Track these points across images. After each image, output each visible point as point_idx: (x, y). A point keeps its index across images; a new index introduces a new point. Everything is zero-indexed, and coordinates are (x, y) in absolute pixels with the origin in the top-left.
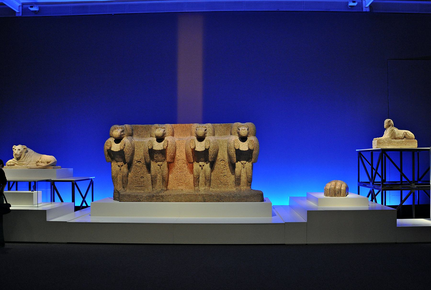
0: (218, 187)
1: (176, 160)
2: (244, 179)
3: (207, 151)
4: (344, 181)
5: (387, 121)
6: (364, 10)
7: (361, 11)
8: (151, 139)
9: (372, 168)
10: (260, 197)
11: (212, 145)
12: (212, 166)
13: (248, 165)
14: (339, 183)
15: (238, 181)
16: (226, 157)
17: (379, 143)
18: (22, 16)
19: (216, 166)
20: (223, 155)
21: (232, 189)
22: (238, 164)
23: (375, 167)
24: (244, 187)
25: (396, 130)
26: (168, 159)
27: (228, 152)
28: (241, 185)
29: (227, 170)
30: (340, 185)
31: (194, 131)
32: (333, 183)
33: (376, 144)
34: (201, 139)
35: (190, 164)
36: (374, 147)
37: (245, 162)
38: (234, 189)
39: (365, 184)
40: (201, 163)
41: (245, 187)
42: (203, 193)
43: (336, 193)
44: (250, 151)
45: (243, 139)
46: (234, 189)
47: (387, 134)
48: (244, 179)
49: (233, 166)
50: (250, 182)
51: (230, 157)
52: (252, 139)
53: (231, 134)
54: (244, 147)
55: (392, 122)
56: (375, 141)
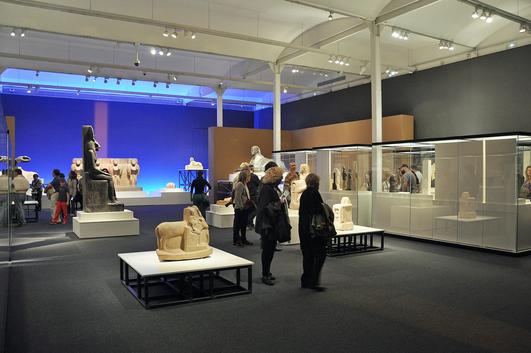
0: (123, 186)
2: (133, 182)
3: (119, 170)
4: (174, 183)
5: (191, 158)
6: (184, 105)
7: (182, 105)
9: (185, 178)
10: (141, 189)
12: (120, 176)
13: (135, 176)
14: (172, 183)
15: (131, 183)
16: (126, 173)
17: (188, 167)
18: (3, 93)
20: (125, 172)
21: (129, 186)
22: (131, 176)
23: (186, 177)
24: (133, 185)
25: (195, 162)
27: (127, 171)
28: (132, 184)
29: (127, 178)
30: (173, 184)
32: (170, 183)
33: (187, 168)
34: (116, 165)
35: (129, 177)
36: (186, 169)
37: (134, 175)
38: (130, 186)
39: (182, 185)
40: (115, 175)
41: (134, 185)
42: (117, 188)
43: (171, 187)
44: (137, 171)
45: (134, 165)
46: (130, 186)
47: (191, 163)
48: (133, 182)
49: (129, 177)
50: (136, 183)
51: (128, 173)
52: (137, 165)
53: (128, 163)
54: (134, 169)
55: (193, 159)
56: (186, 166)
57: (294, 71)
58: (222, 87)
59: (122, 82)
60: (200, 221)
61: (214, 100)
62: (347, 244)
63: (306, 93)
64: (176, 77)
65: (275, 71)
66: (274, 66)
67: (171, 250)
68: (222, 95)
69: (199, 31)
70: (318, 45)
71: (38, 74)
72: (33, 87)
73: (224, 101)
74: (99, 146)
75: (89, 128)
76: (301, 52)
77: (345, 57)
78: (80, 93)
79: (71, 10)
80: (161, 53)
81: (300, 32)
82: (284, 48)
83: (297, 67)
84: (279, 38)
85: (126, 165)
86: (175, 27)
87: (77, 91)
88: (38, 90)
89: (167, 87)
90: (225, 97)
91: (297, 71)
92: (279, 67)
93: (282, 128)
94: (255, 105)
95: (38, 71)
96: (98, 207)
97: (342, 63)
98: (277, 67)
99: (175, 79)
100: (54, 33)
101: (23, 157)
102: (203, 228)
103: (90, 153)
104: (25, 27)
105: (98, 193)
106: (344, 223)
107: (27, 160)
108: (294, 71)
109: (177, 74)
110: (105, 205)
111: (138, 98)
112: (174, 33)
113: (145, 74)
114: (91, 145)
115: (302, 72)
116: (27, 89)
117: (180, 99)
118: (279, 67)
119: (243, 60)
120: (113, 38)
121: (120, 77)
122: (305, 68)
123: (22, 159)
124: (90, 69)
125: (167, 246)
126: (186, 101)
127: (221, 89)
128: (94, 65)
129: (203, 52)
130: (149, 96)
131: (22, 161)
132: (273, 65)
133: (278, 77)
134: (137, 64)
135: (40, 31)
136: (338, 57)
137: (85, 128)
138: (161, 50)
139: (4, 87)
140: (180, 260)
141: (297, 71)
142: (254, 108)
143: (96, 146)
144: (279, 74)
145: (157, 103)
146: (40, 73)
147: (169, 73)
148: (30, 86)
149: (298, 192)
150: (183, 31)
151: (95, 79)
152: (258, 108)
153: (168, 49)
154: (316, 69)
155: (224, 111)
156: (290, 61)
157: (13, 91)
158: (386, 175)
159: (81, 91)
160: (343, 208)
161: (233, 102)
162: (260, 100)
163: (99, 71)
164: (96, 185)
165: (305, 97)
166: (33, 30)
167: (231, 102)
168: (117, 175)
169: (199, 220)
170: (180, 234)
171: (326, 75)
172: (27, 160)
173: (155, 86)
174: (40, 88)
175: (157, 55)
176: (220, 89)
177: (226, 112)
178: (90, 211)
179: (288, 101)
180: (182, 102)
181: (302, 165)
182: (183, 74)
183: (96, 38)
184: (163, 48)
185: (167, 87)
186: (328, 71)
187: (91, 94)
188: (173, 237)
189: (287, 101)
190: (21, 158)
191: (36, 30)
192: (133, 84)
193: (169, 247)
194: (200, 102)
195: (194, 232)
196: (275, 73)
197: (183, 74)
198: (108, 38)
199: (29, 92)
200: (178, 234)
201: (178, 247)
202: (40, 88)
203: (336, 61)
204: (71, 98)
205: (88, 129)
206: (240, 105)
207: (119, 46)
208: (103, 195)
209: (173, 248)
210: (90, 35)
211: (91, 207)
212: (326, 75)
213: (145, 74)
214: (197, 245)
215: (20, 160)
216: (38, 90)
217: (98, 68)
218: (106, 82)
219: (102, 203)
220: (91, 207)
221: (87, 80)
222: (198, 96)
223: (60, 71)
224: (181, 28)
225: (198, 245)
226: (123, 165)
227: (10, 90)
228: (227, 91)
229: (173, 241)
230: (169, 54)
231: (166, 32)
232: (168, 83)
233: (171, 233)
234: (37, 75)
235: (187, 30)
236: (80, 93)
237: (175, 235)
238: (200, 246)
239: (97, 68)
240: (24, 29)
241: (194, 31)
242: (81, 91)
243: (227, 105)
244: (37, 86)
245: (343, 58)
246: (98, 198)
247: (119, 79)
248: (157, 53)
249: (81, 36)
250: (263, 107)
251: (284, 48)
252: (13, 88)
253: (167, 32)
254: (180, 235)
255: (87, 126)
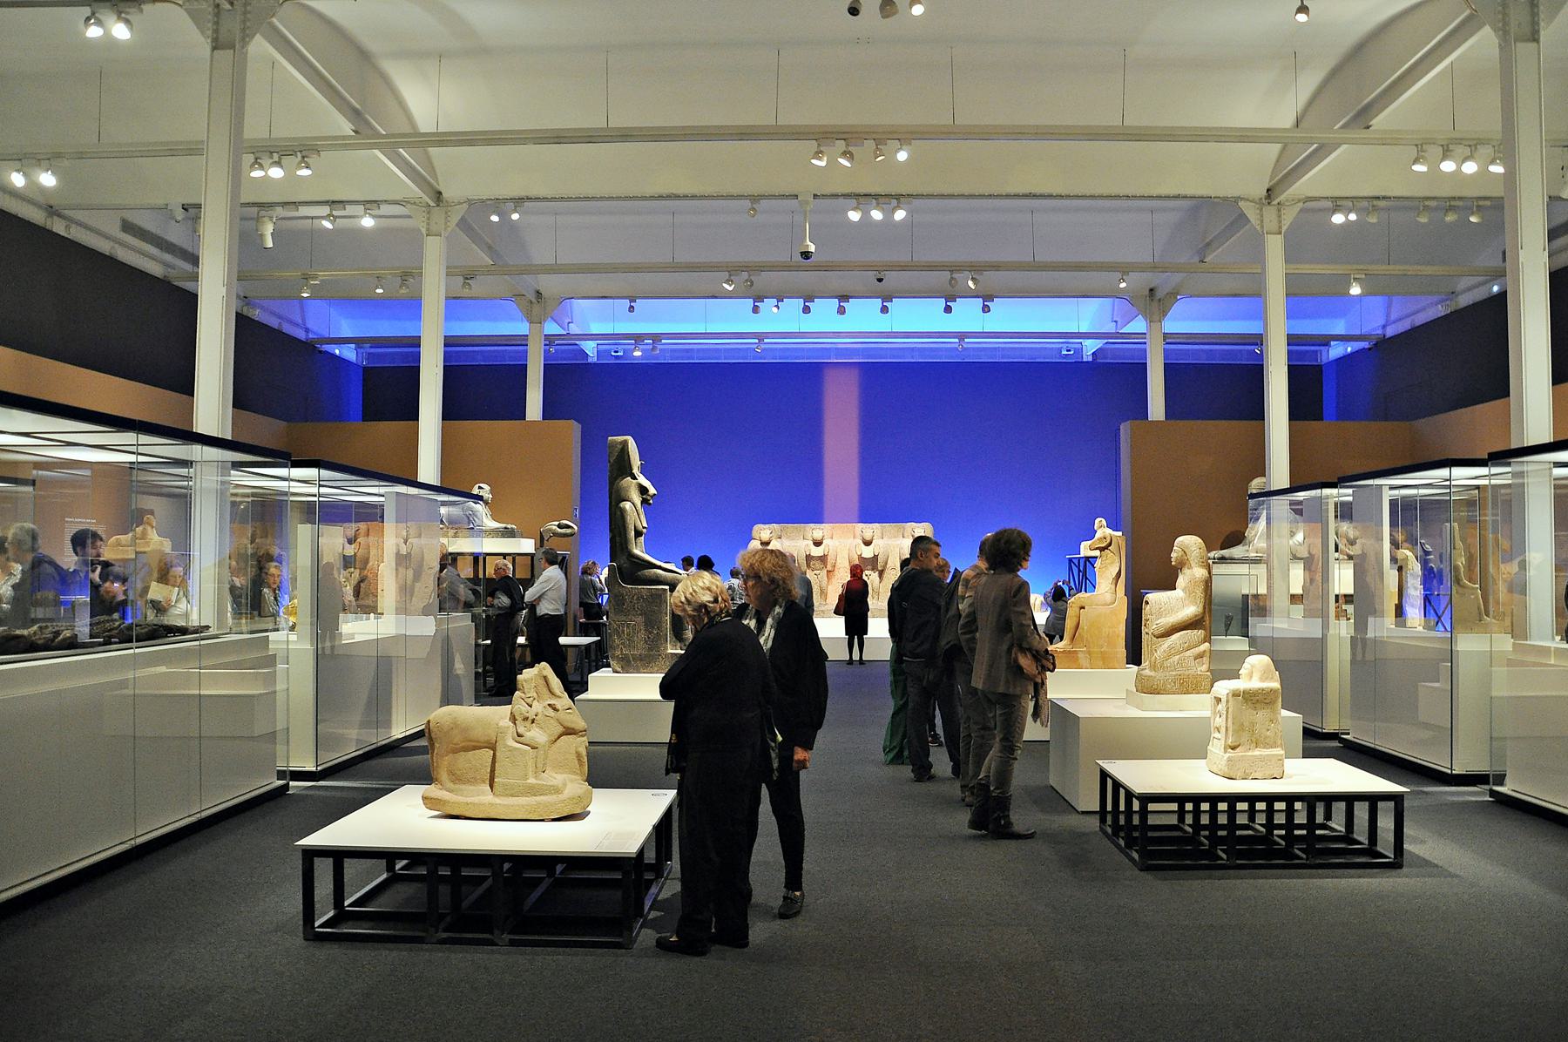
1: (836, 569)
3: (876, 557)
8: (806, 542)
11: (882, 551)
19: (885, 575)
26: (829, 568)
31: (858, 532)
34: (868, 543)
55: (1104, 522)
57: (1338, 219)
58: (1159, 294)
59: (851, 305)
60: (550, 709)
61: (522, 341)
62: (1205, 830)
63: (1469, 289)
64: (973, 279)
65: (1262, 227)
66: (1261, 210)
67: (463, 787)
68: (1161, 322)
69: (919, 136)
70: (1363, 117)
71: (633, 307)
72: (646, 341)
73: (550, 340)
74: (652, 491)
75: (621, 443)
76: (1322, 151)
77: (1432, 142)
78: (763, 346)
79: (559, 138)
80: (877, 215)
81: (1309, 82)
82: (1279, 146)
83: (1351, 204)
84: (1245, 115)
85: (899, 542)
86: (874, 136)
87: (757, 341)
88: (659, 347)
89: (984, 311)
90: (1176, 323)
91: (1353, 217)
92: (1279, 210)
93: (1294, 415)
94: (1327, 344)
95: (633, 300)
96: (641, 658)
97: (1470, 168)
98: (1270, 213)
99: (971, 284)
100: (587, 199)
101: (557, 523)
102: (560, 729)
103: (623, 512)
104: (1042, 192)
105: (640, 619)
106: (1239, 752)
107: (569, 531)
108: (1338, 219)
109: (976, 269)
110: (660, 655)
111: (947, 349)
112: (844, 154)
113: (880, 280)
114: (627, 489)
115: (1373, 219)
116: (633, 347)
117: (1073, 343)
118: (1279, 210)
119: (1194, 202)
120: (735, 192)
121: (989, 293)
122: (1382, 204)
123: (554, 527)
124: (727, 282)
125: (451, 773)
126: (1090, 347)
127: (1160, 300)
128: (737, 268)
129: (1008, 196)
130: (957, 340)
131: (556, 534)
132: (1257, 206)
133: (1275, 247)
134: (806, 255)
135: (553, 199)
136: (1451, 147)
137: (614, 444)
138: (877, 207)
139: (600, 347)
140: (480, 817)
141: (1353, 217)
142: (1324, 353)
143: (643, 490)
144: (1280, 233)
145: (1002, 358)
146: (638, 304)
147: (954, 268)
148: (638, 338)
149: (1156, 633)
150: (870, 144)
151: (777, 307)
152: (1336, 351)
153: (899, 199)
154: (1427, 203)
155: (1168, 368)
156: (1305, 185)
157: (618, 354)
158: (683, 560)
159: (766, 341)
160: (1233, 695)
161: (1247, 341)
162: (1339, 328)
163: (752, 283)
164: (635, 597)
165: (1464, 300)
166: (537, 199)
167: (1243, 341)
168: (873, 570)
169: (549, 705)
170: (485, 742)
171: (1473, 219)
172: (569, 531)
173: (948, 309)
174: (663, 341)
175: (1348, 224)
176: (1155, 301)
177: (453, 376)
178: (619, 670)
179: (1416, 320)
180: (1079, 351)
181: (1180, 539)
182: (996, 267)
183: (684, 196)
184: (881, 200)
185: (986, 309)
186: (1481, 203)
187: (1135, 346)
188: (466, 749)
189: (1413, 320)
190: (553, 525)
191: (545, 199)
192: (986, 309)
193: (457, 778)
194: (1127, 346)
195: (519, 739)
196: (1263, 232)
197: (996, 267)
198: (724, 192)
199: (637, 354)
200: (478, 742)
201: (484, 782)
202: (663, 341)
203: (1443, 160)
204: (691, 361)
205: (620, 447)
206: (1252, 347)
207: (753, 209)
208: (653, 627)
209: (468, 782)
210: (943, 193)
211: (623, 659)
212: (1473, 219)
213: (880, 280)
214: (529, 781)
215: (550, 530)
216: (659, 347)
217: (750, 276)
218: (884, 310)
219: (650, 649)
220: (623, 659)
221: (755, 310)
222: (1110, 328)
223: (645, 293)
224: (861, 135)
225: (532, 780)
226: (890, 542)
227: (1065, 352)
228: (1177, 309)
229: (467, 760)
230: (900, 215)
231: (818, 154)
232: (987, 298)
233: (457, 738)
234: (631, 309)
235: (883, 137)
236: (763, 346)
237: (473, 744)
238: (540, 782)
239: (745, 275)
240: (519, 202)
241: (905, 136)
242: (766, 341)
243: (1232, 350)
244: (657, 338)
245: (1476, 148)
246: (642, 635)
247: (844, 298)
248: (866, 214)
249: (652, 198)
250: (1349, 349)
251: (1279, 146)
252: (1069, 345)
253: (821, 152)
254: (485, 745)
255: (619, 437)
